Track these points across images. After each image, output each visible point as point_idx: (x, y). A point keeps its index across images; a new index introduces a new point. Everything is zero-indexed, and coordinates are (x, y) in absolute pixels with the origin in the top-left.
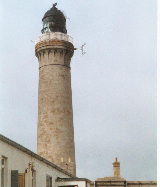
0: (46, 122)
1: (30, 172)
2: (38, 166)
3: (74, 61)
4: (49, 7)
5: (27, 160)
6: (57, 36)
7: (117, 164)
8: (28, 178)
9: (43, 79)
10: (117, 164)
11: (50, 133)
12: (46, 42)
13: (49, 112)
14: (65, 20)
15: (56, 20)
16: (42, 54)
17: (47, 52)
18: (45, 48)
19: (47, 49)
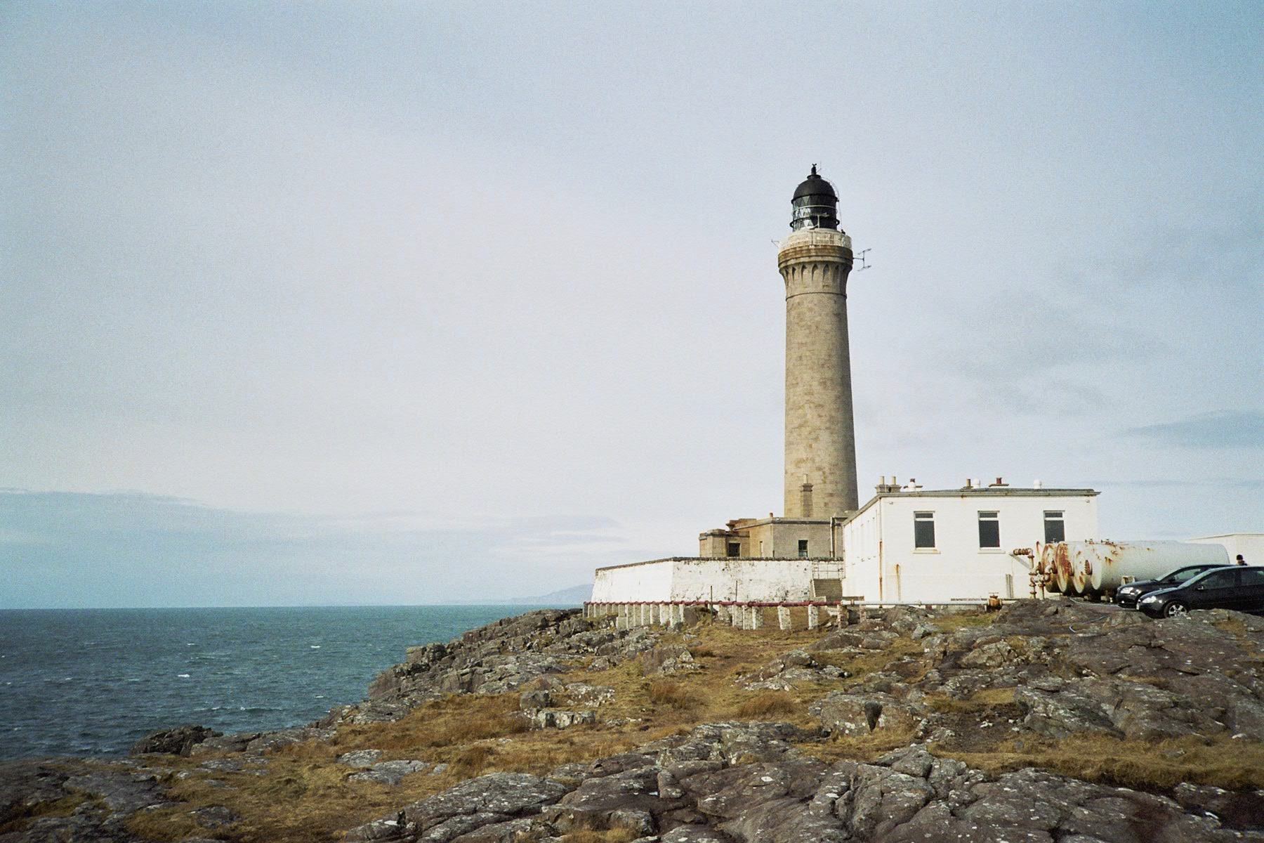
0: (809, 402)
6: (823, 236)
11: (818, 423)
12: (809, 250)
13: (815, 383)
15: (819, 198)
16: (790, 271)
18: (807, 260)
19: (810, 263)
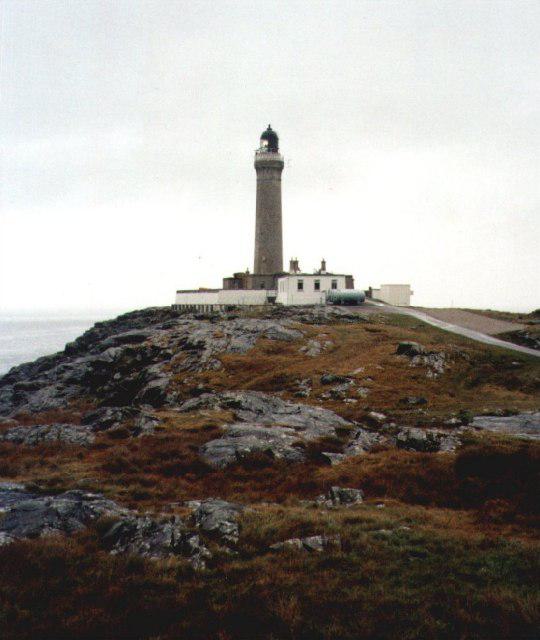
15: (271, 137)
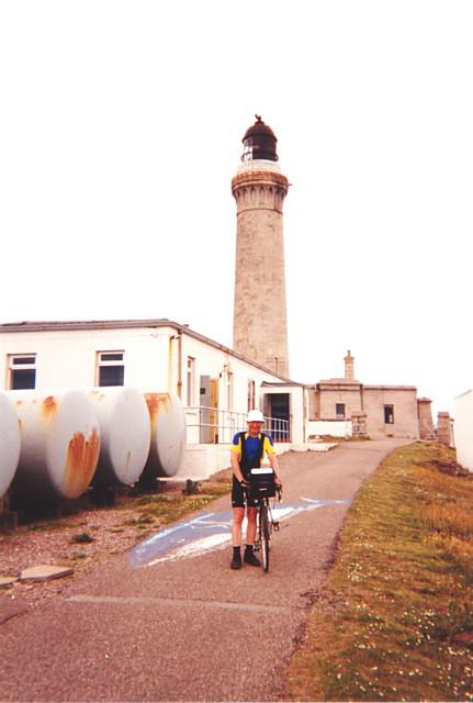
1: (225, 375)
2: (236, 365)
3: (288, 203)
4: (252, 122)
5: (221, 357)
6: (264, 165)
7: (349, 360)
8: (223, 385)
9: (243, 231)
10: (349, 360)
12: (247, 176)
14: (276, 140)
15: (261, 140)
16: (241, 193)
17: (248, 190)
18: (246, 184)
19: (248, 186)
